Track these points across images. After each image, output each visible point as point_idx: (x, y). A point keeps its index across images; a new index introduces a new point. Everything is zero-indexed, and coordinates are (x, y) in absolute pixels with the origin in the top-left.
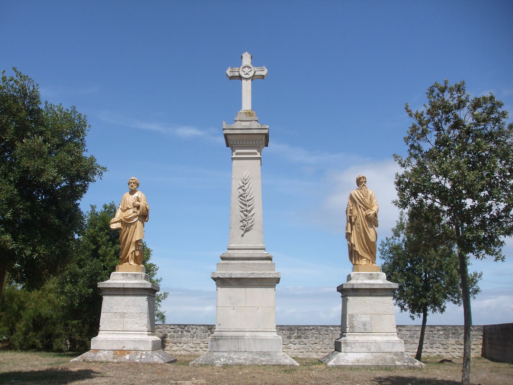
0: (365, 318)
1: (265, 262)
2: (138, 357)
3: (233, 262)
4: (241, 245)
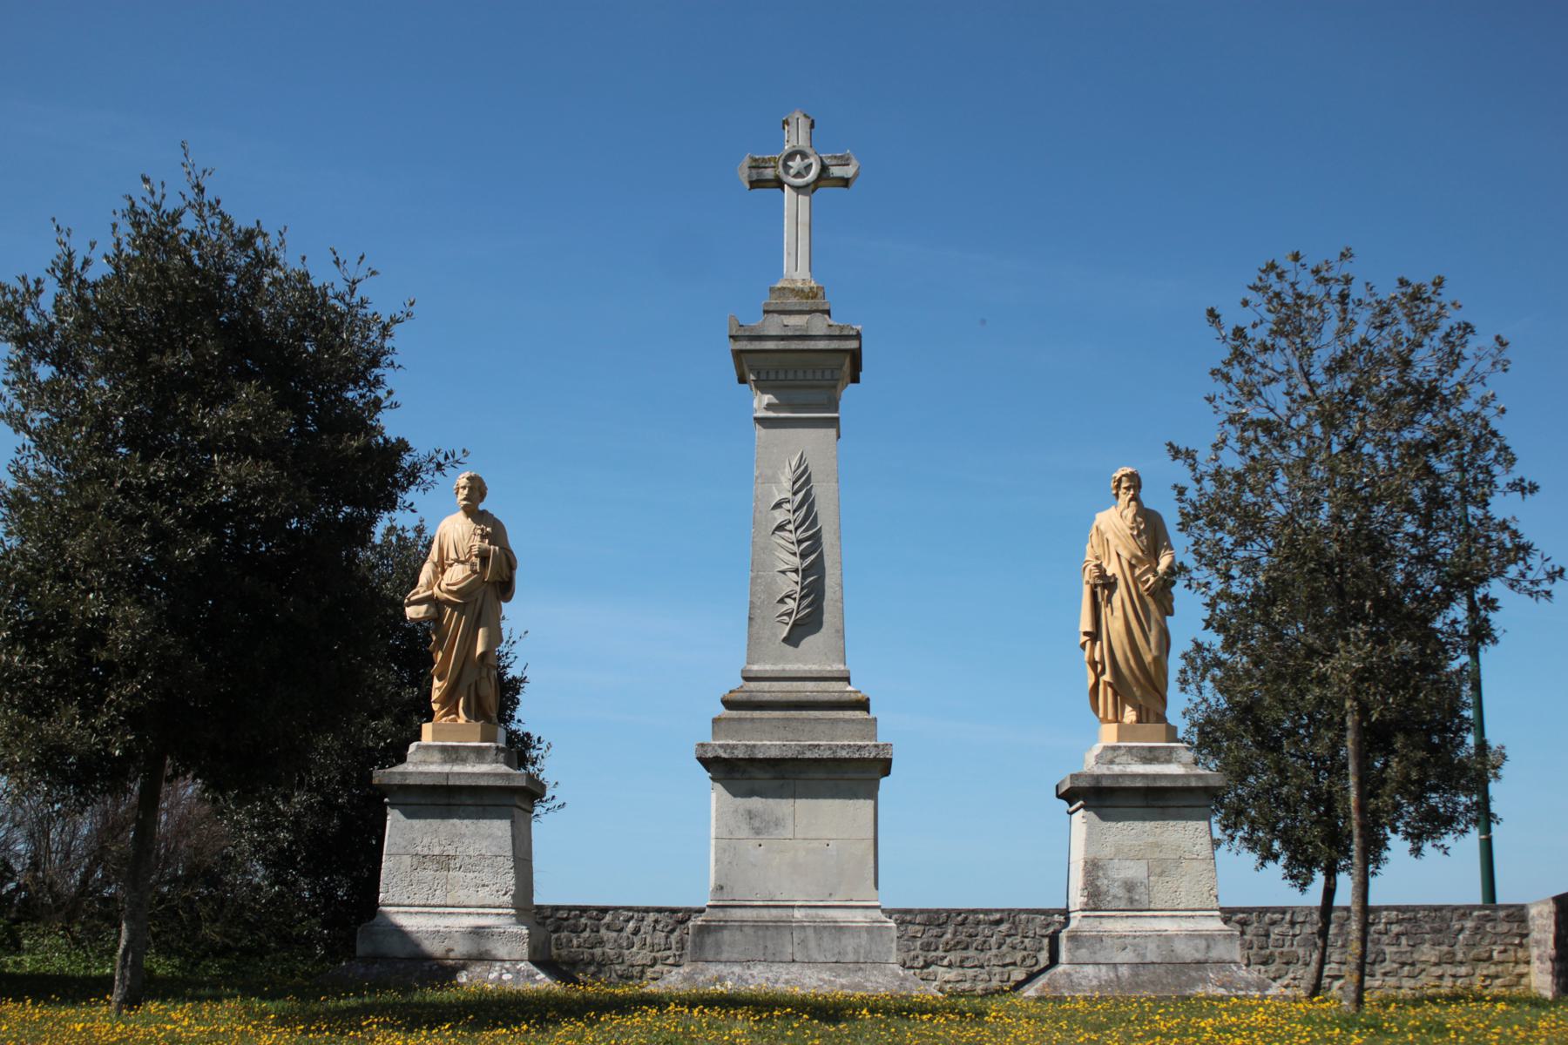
0: (1134, 870)
1: (848, 714)
2: (491, 976)
3: (805, 714)
4: (779, 667)
